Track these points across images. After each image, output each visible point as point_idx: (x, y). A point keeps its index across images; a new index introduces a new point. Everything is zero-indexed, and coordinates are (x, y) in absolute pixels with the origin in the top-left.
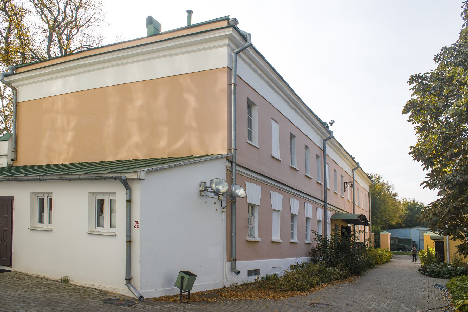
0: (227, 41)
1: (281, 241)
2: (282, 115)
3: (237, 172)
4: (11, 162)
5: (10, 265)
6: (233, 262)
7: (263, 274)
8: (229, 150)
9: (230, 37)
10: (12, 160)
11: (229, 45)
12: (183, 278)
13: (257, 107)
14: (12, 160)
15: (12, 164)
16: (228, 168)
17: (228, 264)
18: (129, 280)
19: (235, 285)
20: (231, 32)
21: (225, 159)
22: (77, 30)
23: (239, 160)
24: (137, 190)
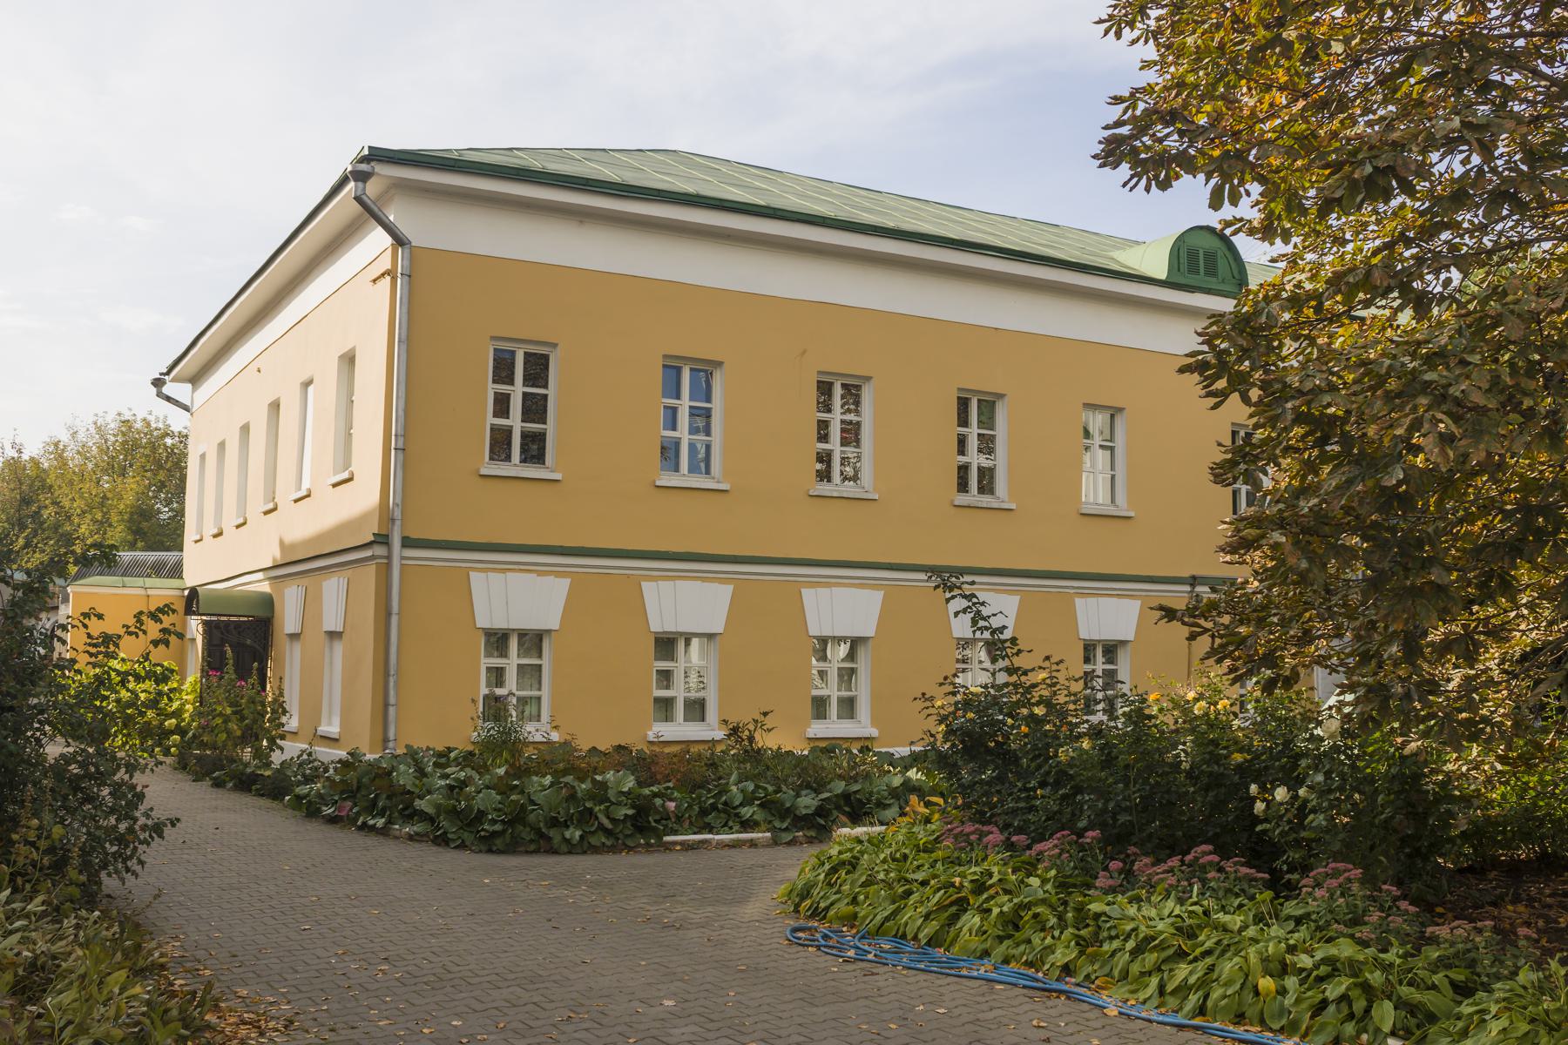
2: (700, 492)
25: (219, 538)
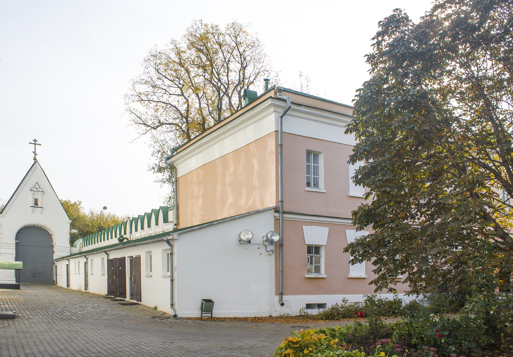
0: (272, 109)
1: (366, 277)
3: (284, 219)
4: (175, 227)
5: (141, 301)
6: (281, 295)
7: (329, 306)
8: (277, 202)
9: (272, 105)
10: (175, 225)
11: (275, 111)
12: (202, 303)
13: (323, 154)
14: (175, 225)
15: (177, 228)
16: (277, 218)
17: (277, 298)
18: (172, 305)
19: (286, 315)
20: (271, 102)
21: (273, 211)
22: (233, 103)
23: (287, 207)
24: (176, 245)
25: (170, 306)
